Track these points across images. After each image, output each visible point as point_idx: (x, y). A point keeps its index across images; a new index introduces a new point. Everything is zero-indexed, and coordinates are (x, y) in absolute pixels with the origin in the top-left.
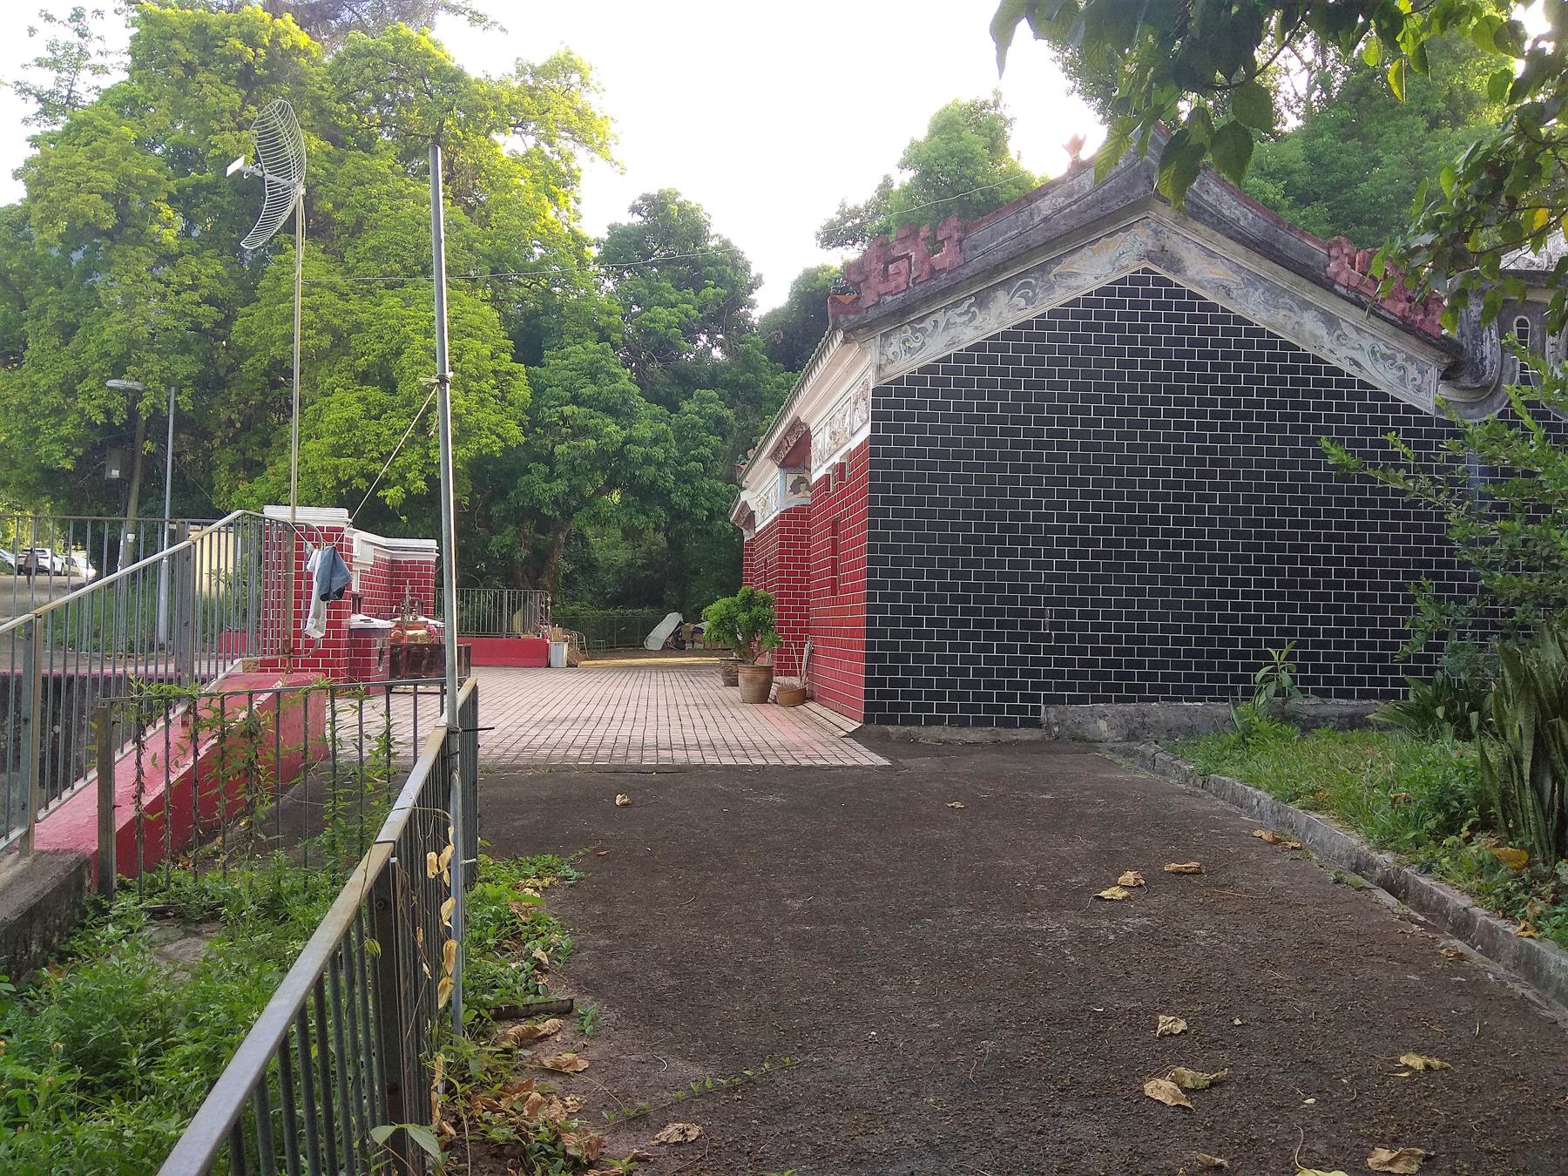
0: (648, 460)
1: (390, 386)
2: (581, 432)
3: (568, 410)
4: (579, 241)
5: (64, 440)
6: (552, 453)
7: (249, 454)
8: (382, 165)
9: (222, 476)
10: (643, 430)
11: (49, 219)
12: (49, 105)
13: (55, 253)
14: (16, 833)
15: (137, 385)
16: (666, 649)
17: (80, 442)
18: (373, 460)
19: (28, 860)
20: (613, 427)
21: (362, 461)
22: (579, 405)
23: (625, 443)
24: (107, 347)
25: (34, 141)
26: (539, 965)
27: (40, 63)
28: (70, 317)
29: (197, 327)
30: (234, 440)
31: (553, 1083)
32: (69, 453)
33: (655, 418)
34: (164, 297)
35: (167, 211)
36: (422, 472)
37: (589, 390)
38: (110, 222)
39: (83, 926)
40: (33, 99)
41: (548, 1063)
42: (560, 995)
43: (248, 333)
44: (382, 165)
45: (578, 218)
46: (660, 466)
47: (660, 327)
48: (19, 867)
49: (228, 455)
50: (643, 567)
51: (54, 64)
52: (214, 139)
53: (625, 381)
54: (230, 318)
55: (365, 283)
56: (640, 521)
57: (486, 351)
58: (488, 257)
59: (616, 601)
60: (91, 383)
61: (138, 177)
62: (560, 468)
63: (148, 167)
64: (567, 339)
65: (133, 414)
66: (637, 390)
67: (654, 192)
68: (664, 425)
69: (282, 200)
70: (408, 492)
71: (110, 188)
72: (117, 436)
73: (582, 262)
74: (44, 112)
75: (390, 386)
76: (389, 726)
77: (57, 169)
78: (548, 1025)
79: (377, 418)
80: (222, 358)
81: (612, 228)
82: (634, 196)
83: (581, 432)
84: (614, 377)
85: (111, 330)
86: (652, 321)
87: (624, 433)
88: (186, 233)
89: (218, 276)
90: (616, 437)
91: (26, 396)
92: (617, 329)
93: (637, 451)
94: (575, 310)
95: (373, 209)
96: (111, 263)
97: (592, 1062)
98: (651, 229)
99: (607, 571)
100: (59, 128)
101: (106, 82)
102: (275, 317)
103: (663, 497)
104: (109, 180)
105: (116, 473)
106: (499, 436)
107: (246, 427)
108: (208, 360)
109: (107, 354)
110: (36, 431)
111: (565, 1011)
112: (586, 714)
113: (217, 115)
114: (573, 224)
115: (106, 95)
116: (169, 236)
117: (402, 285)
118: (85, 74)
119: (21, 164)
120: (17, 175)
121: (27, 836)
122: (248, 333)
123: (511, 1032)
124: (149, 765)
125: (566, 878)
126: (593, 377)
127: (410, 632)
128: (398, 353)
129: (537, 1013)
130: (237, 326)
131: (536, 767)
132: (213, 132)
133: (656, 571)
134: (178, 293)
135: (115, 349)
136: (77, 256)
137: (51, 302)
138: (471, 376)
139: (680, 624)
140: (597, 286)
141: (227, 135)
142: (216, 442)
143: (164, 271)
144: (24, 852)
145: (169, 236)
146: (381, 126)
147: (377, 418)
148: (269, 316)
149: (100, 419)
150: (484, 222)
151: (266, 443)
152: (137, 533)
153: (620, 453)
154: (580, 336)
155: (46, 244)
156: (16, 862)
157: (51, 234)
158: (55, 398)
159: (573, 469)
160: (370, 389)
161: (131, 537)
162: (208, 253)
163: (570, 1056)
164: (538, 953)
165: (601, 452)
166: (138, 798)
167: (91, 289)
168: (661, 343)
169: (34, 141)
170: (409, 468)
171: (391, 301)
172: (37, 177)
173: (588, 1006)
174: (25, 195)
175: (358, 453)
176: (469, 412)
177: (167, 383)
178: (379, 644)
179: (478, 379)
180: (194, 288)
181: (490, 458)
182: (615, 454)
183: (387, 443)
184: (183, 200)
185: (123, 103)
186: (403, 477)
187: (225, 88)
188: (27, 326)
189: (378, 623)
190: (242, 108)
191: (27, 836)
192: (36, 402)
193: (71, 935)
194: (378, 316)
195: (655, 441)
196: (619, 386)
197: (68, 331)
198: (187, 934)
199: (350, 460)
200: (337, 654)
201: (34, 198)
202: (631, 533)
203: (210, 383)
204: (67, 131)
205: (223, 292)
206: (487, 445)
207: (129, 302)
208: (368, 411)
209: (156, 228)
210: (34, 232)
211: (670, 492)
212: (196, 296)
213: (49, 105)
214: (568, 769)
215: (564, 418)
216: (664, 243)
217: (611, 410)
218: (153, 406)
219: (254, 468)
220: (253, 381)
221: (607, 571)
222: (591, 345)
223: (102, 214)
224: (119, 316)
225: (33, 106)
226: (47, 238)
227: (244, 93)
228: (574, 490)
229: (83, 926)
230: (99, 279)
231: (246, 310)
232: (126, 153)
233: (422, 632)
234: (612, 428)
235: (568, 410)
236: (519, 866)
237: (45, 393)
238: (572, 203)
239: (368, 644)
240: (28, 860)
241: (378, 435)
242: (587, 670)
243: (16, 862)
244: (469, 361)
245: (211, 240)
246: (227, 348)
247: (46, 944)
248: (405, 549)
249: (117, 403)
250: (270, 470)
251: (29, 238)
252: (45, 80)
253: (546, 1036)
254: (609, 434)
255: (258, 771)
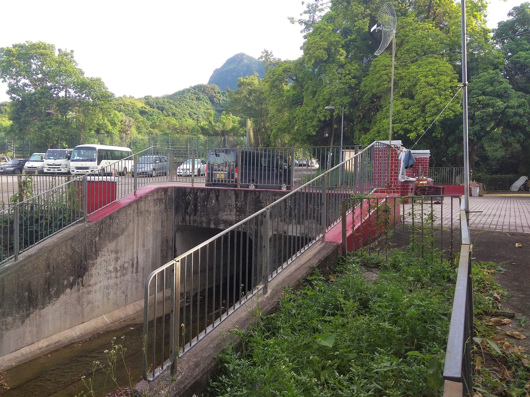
0: (516, 114)
1: (412, 97)
2: (488, 105)
3: (481, 98)
4: (486, 31)
5: (313, 126)
6: (474, 115)
7: (365, 126)
8: (410, 20)
9: (357, 133)
10: (514, 102)
11: (310, 60)
12: (308, 25)
13: (311, 70)
14: (321, 236)
15: (333, 107)
16: (520, 191)
17: (317, 126)
18: (406, 124)
19: (324, 244)
20: (501, 103)
21: (402, 125)
22: (485, 95)
23: (505, 109)
24: (325, 97)
25: (305, 37)
26: (496, 299)
27: (305, 12)
28: (315, 89)
29: (350, 87)
30: (360, 122)
31: (513, 341)
32: (315, 130)
33: (519, 97)
34: (340, 79)
35: (342, 51)
36: (423, 126)
37: (491, 89)
38: (326, 57)
39: (339, 264)
40: (303, 24)
41: (508, 333)
42: (508, 311)
43: (365, 86)
44: (410, 20)
45: (485, 22)
46: (521, 116)
47: (522, 60)
48: (322, 245)
49: (359, 126)
50: (509, 158)
51: (308, 12)
52: (356, 23)
53: (506, 84)
54: (360, 83)
55: (404, 62)
56: (511, 139)
57: (448, 80)
58: (449, 45)
59: (496, 172)
60: (321, 108)
61: (334, 41)
62: (477, 120)
63: (337, 37)
64: (480, 71)
65: (332, 116)
66: (511, 86)
67: (518, 5)
68: (523, 100)
69: (387, 35)
70: (418, 134)
71: (326, 47)
72: (326, 124)
73: (486, 40)
74: (306, 28)
75: (412, 97)
76: (432, 211)
77: (312, 44)
78: (506, 320)
79: (408, 109)
80: (356, 95)
81: (499, 24)
82: (510, 9)
83: (488, 105)
84: (501, 83)
85: (326, 91)
86: (518, 58)
87: (505, 105)
88: (347, 57)
89: (356, 69)
90: (502, 106)
91: (304, 114)
92: (502, 63)
93: (511, 111)
94: (483, 59)
95: (407, 36)
96: (326, 71)
97: (527, 337)
98: (518, 21)
99: (493, 160)
100: (311, 31)
101: (323, 14)
102: (374, 79)
103: (522, 129)
104: (325, 44)
105: (327, 135)
106: (452, 111)
107: (364, 117)
108: (353, 97)
109: (325, 99)
110: (306, 124)
111: (512, 317)
112: (493, 213)
113: (356, 16)
114: (483, 26)
115: (323, 18)
116: (342, 59)
117: (416, 61)
118: (317, 13)
119: (302, 45)
120: (301, 49)
121: (323, 237)
122: (365, 86)
123: (492, 319)
124: (355, 218)
125: (500, 271)
126: (492, 84)
127: (421, 182)
128: (415, 85)
129: (500, 315)
130: (362, 84)
131: (479, 231)
132: (356, 21)
133: (515, 160)
134: (345, 77)
135: (327, 97)
136: (316, 70)
137: (309, 85)
138: (442, 90)
139: (527, 181)
140: (493, 48)
141: (360, 21)
142: (355, 123)
143: (340, 71)
144: (323, 242)
145: (342, 59)
146: (410, 6)
147: (408, 109)
148: (372, 79)
149: (323, 119)
150: (447, 32)
151: (370, 122)
152: (333, 153)
153: (503, 113)
154: (486, 69)
155: (309, 68)
156: (321, 244)
157: (310, 65)
158: (311, 114)
159: (483, 120)
160: (405, 99)
161: (331, 154)
162: (353, 62)
163: (517, 333)
164: (496, 295)
165: (495, 113)
166: (353, 228)
167: (321, 79)
168: (522, 66)
169: (305, 37)
170: (418, 125)
171: (413, 67)
172: (306, 48)
173: (518, 316)
174: (303, 54)
175: (401, 122)
176: (441, 103)
177: (341, 106)
178: (411, 186)
179: (445, 91)
180: (349, 74)
181: (449, 119)
182: (501, 113)
183: (410, 117)
184: (346, 46)
185: (329, 19)
186: (416, 129)
187: (359, 6)
188: (304, 93)
189: (411, 179)
190: (365, 11)
191: (323, 237)
192: (306, 116)
193: (336, 266)
194: (408, 73)
195: (519, 106)
196: (503, 86)
197: (314, 93)
198: (368, 271)
199: (398, 124)
200: (397, 189)
201: (306, 54)
202: (506, 145)
203: (354, 104)
204: (313, 32)
205: (358, 74)
206: (448, 115)
207: (331, 81)
208: (404, 107)
209: (339, 57)
210: (305, 65)
211: (525, 126)
212: (350, 77)
213: (308, 25)
214: (492, 232)
215: (479, 101)
216: (523, 25)
217: (500, 96)
218: (338, 113)
219: (366, 130)
220: (367, 101)
221: (493, 160)
222: (491, 71)
223: (324, 55)
224: (328, 86)
225: (303, 26)
226: (309, 66)
227: (365, 5)
228: (483, 129)
229: (339, 264)
230: (322, 76)
231: (365, 79)
232: (330, 34)
233: (425, 182)
234: (500, 103)
235: (481, 98)
236: (480, 264)
237: (309, 113)
238: (483, 17)
239: (408, 186)
240: (324, 244)
241: (407, 115)
242: (487, 198)
243: (321, 244)
244: (441, 84)
245: (355, 57)
246: (358, 92)
247: (330, 268)
248: (419, 154)
249: (328, 114)
250: (372, 130)
251: (304, 67)
252: (306, 17)
253: (505, 324)
254: (498, 105)
255: (389, 223)
